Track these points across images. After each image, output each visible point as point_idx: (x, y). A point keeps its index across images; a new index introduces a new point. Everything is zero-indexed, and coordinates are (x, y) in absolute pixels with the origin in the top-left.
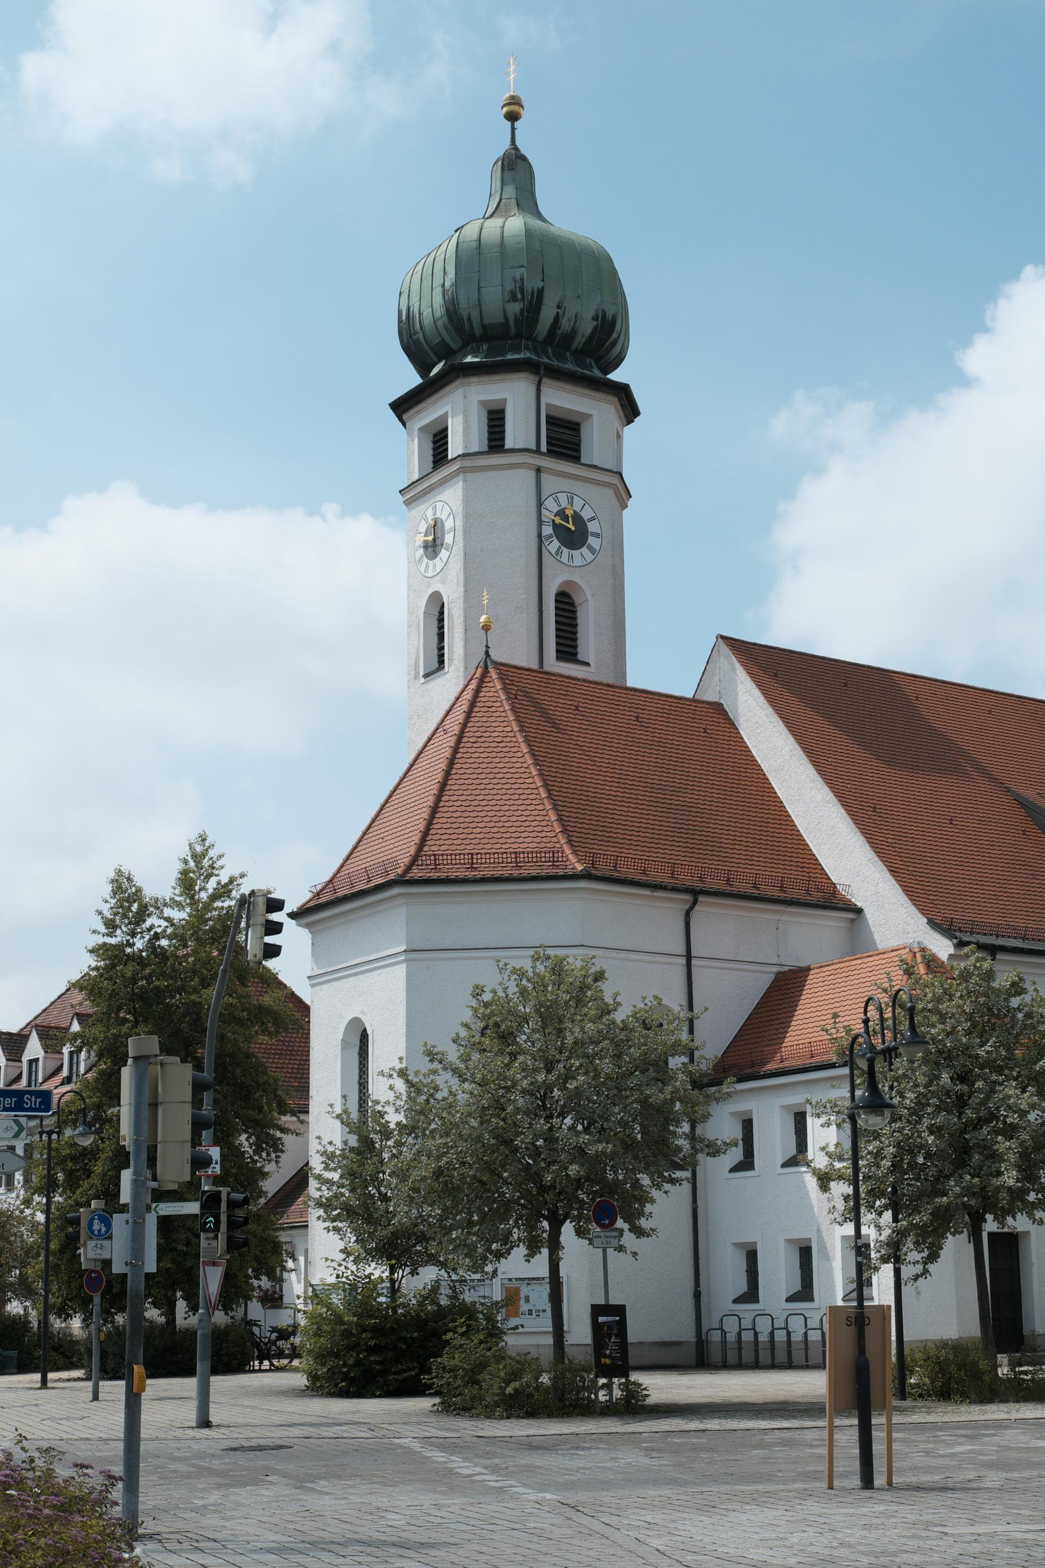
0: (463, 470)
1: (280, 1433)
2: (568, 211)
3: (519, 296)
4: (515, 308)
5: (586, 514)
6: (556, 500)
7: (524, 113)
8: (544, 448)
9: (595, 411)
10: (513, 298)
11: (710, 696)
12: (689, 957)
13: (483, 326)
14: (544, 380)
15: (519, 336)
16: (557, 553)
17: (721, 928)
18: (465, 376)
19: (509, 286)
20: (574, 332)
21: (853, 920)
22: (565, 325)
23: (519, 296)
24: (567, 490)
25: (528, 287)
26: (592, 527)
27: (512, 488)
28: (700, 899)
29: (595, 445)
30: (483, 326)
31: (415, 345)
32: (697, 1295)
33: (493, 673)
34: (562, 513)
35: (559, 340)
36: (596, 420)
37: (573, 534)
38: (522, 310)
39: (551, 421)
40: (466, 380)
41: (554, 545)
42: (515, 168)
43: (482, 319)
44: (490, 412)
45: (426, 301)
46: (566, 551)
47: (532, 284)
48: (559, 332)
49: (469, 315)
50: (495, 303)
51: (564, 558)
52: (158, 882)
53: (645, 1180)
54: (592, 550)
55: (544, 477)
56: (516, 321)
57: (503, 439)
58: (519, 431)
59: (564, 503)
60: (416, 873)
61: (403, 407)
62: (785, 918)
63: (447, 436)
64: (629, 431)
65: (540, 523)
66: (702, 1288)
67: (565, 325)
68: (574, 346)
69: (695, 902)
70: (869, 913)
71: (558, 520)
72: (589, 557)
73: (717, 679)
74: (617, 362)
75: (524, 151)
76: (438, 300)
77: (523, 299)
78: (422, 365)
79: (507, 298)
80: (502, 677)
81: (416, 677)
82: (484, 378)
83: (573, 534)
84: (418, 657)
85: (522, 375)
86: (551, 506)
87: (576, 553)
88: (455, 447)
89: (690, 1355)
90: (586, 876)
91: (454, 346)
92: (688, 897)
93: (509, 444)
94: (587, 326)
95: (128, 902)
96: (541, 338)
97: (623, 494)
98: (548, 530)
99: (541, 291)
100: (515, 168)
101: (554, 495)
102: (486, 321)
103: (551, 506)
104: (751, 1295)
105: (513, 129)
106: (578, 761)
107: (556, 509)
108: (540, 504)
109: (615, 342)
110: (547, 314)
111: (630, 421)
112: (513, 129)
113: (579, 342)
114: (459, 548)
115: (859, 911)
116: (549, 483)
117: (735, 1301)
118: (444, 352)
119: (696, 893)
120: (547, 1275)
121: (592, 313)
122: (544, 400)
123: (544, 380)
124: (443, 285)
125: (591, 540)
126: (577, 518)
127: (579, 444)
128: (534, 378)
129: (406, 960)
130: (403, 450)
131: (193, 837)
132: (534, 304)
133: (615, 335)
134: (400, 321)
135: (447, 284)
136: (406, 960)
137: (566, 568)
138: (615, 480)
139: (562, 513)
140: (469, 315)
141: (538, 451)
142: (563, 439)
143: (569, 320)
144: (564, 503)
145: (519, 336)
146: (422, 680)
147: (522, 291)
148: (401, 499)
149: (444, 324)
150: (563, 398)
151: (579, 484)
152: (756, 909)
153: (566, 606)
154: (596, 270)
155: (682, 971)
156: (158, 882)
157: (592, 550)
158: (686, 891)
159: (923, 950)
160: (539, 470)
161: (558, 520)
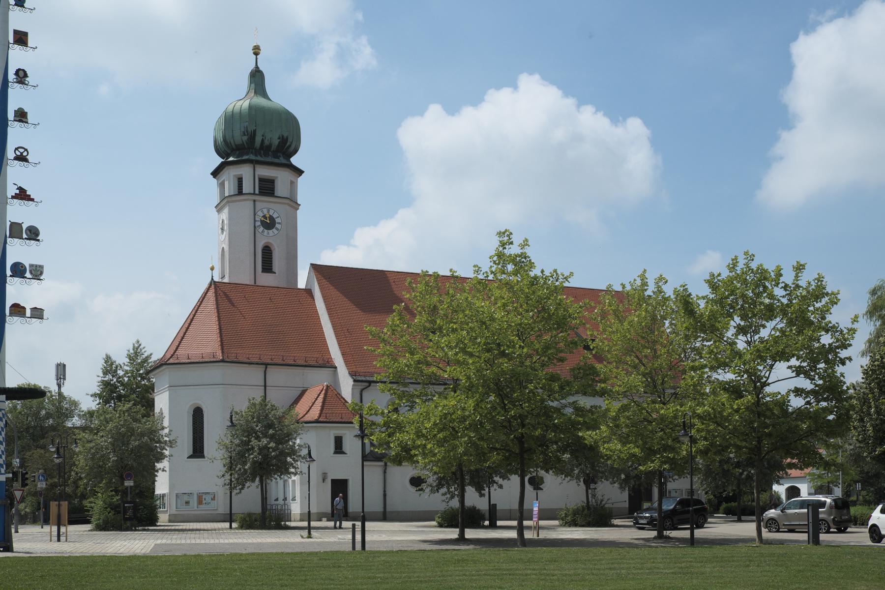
0: (228, 202)
2: (280, 94)
4: (245, 138)
5: (275, 216)
7: (261, 52)
8: (257, 192)
9: (281, 176)
11: (309, 287)
12: (265, 386)
17: (277, 376)
19: (243, 130)
22: (267, 143)
25: (249, 130)
26: (277, 220)
27: (245, 207)
29: (281, 189)
33: (213, 286)
34: (264, 217)
35: (265, 149)
39: (261, 180)
42: (257, 77)
47: (251, 128)
50: (239, 138)
51: (265, 234)
52: (121, 359)
53: (742, 323)
54: (277, 229)
59: (265, 211)
60: (171, 361)
65: (255, 221)
67: (267, 143)
75: (261, 69)
80: (215, 288)
83: (269, 224)
86: (260, 214)
87: (270, 231)
88: (245, 190)
90: (222, 361)
94: (276, 142)
95: (110, 367)
97: (295, 205)
98: (258, 224)
99: (255, 131)
100: (257, 77)
103: (260, 214)
106: (254, 312)
109: (290, 146)
110: (258, 139)
113: (274, 148)
116: (259, 205)
119: (266, 365)
125: (277, 226)
126: (271, 218)
127: (274, 188)
131: (134, 341)
132: (252, 136)
137: (266, 237)
139: (264, 217)
141: (254, 194)
142: (267, 188)
150: (265, 172)
153: (267, 252)
156: (121, 359)
157: (277, 229)
160: (254, 201)
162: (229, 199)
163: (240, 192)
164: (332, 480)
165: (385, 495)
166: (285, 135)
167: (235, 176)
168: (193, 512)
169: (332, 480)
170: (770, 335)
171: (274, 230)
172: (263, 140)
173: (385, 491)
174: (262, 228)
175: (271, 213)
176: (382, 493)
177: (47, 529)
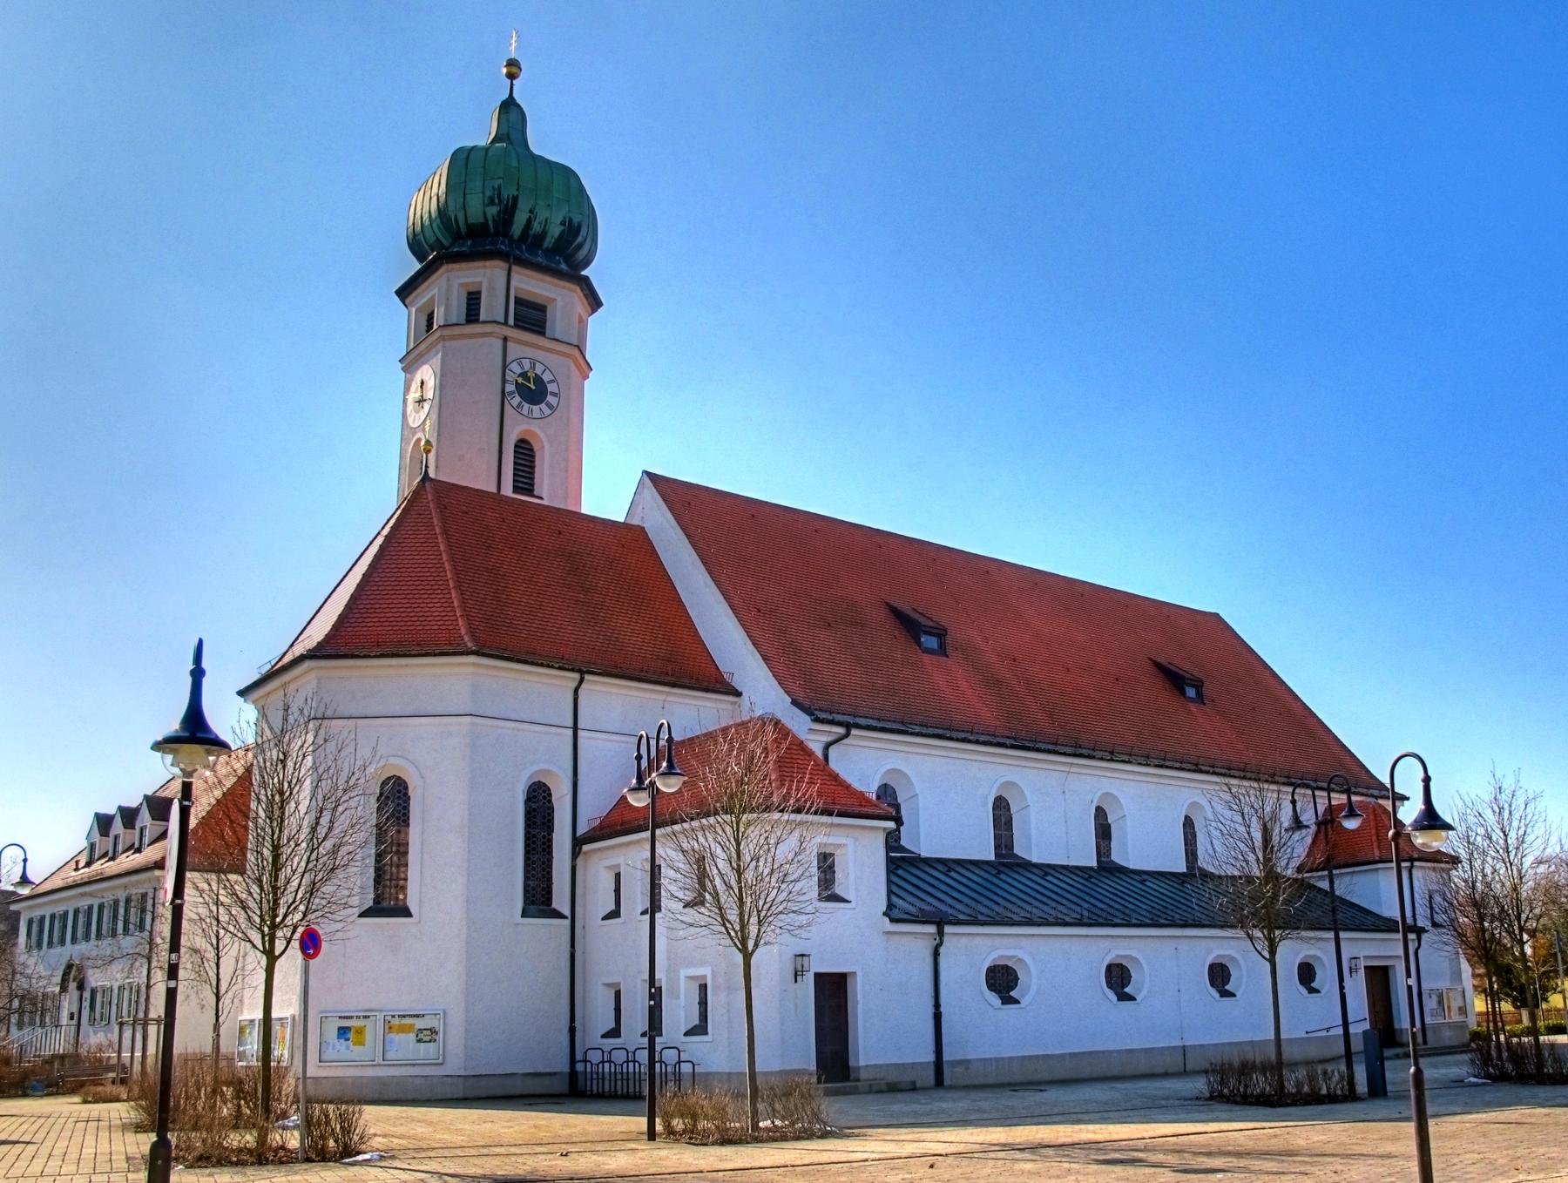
0: (443, 338)
5: (546, 377)
6: (520, 364)
7: (522, 74)
8: (511, 321)
10: (492, 202)
11: (635, 521)
13: (468, 226)
15: (497, 234)
19: (489, 193)
22: (537, 227)
24: (527, 352)
25: (505, 194)
26: (551, 388)
29: (558, 322)
30: (468, 226)
31: (416, 245)
32: (572, 1030)
34: (524, 375)
36: (559, 304)
37: (534, 391)
39: (518, 301)
44: (469, 294)
45: (426, 209)
46: (526, 406)
50: (477, 209)
54: (549, 406)
55: (509, 344)
58: (491, 306)
59: (527, 366)
61: (404, 293)
62: (670, 698)
64: (593, 321)
65: (504, 381)
66: (578, 1024)
67: (537, 227)
68: (546, 245)
69: (581, 681)
71: (520, 380)
72: (547, 411)
74: (587, 262)
78: (420, 256)
82: (464, 265)
83: (534, 391)
87: (536, 408)
89: (561, 1086)
93: (482, 317)
94: (555, 230)
96: (516, 236)
97: (586, 369)
98: (510, 388)
99: (515, 199)
101: (519, 361)
102: (470, 221)
104: (615, 1032)
107: (519, 371)
108: (505, 367)
109: (580, 246)
110: (521, 218)
111: (594, 311)
113: (548, 242)
116: (514, 350)
117: (603, 1036)
118: (437, 246)
121: (560, 219)
122: (513, 283)
125: (549, 398)
126: (538, 380)
128: (504, 265)
130: (398, 322)
132: (509, 210)
133: (580, 239)
138: (576, 352)
139: (524, 375)
141: (506, 323)
142: (531, 317)
144: (527, 366)
145: (497, 234)
148: (400, 366)
150: (531, 284)
152: (417, 666)
154: (565, 182)
157: (549, 406)
159: (777, 723)
160: (505, 339)
161: (520, 380)
162: (447, 332)
163: (472, 315)
164: (816, 975)
165: (937, 1017)
166: (575, 221)
167: (461, 285)
168: (369, 1072)
169: (816, 975)
170: (95, 1033)
171: (543, 406)
172: (529, 222)
173: (937, 1005)
174: (517, 399)
175: (539, 369)
176: (931, 1010)
177: (758, 713)
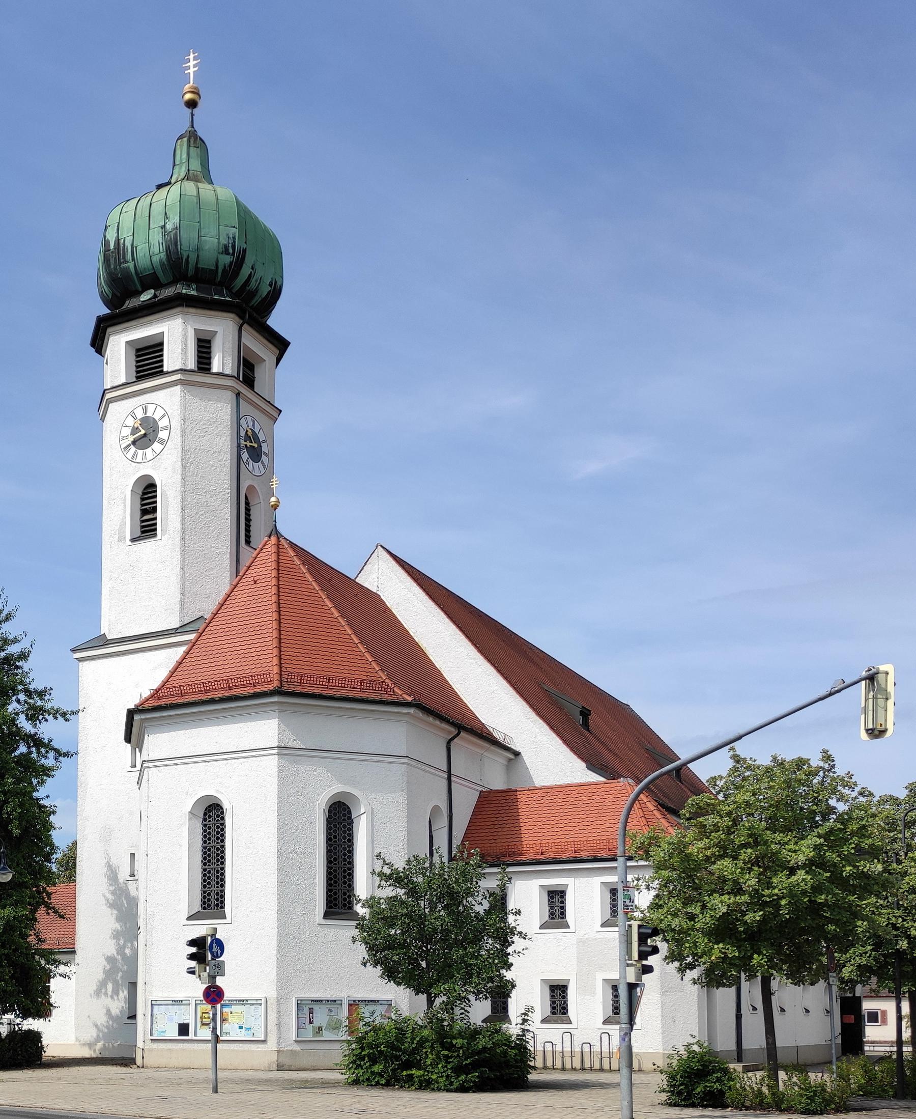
1: (866, 1104)
3: (231, 251)
4: (226, 260)
10: (226, 252)
13: (197, 268)
14: (245, 326)
15: (221, 284)
16: (133, 457)
18: (188, 306)
19: (224, 241)
20: (257, 290)
21: (510, 760)
22: (253, 284)
23: (231, 251)
28: (462, 734)
29: (261, 375)
38: (231, 263)
40: (186, 309)
41: (245, 456)
43: (197, 263)
48: (248, 288)
49: (188, 257)
56: (224, 270)
57: (209, 364)
63: (162, 350)
70: (526, 756)
73: (375, 576)
76: (157, 238)
77: (233, 254)
79: (221, 250)
81: (121, 539)
84: (123, 525)
85: (232, 315)
91: (163, 280)
92: (454, 731)
99: (245, 251)
105: (192, 115)
110: (245, 271)
112: (192, 115)
113: (256, 300)
114: (175, 443)
115: (517, 754)
120: (272, 994)
123: (245, 326)
124: (163, 227)
129: (278, 754)
134: (107, 249)
135: (169, 227)
136: (278, 754)
140: (188, 257)
143: (256, 281)
146: (130, 543)
147: (234, 247)
149: (161, 261)
150: (254, 343)
151: (258, 413)
155: (445, 783)
158: (453, 724)
160: (238, 394)
